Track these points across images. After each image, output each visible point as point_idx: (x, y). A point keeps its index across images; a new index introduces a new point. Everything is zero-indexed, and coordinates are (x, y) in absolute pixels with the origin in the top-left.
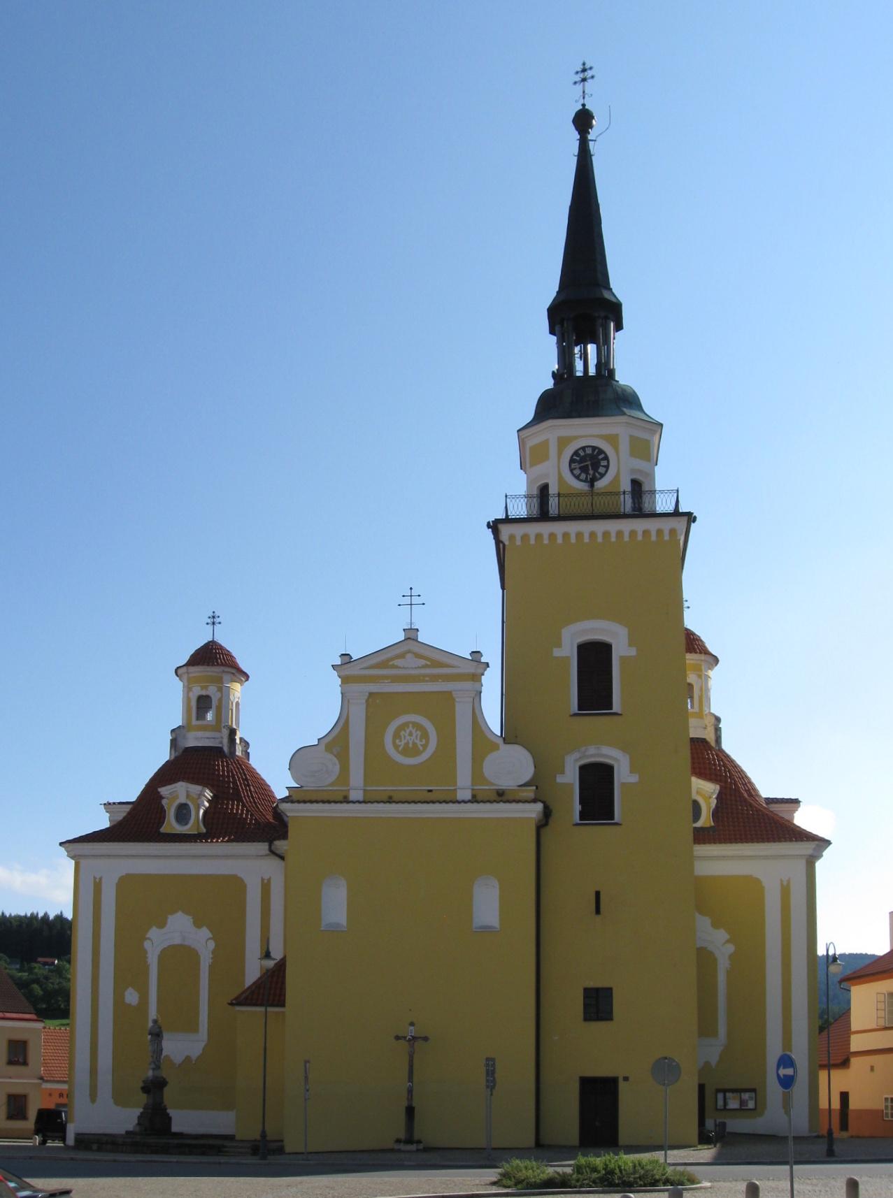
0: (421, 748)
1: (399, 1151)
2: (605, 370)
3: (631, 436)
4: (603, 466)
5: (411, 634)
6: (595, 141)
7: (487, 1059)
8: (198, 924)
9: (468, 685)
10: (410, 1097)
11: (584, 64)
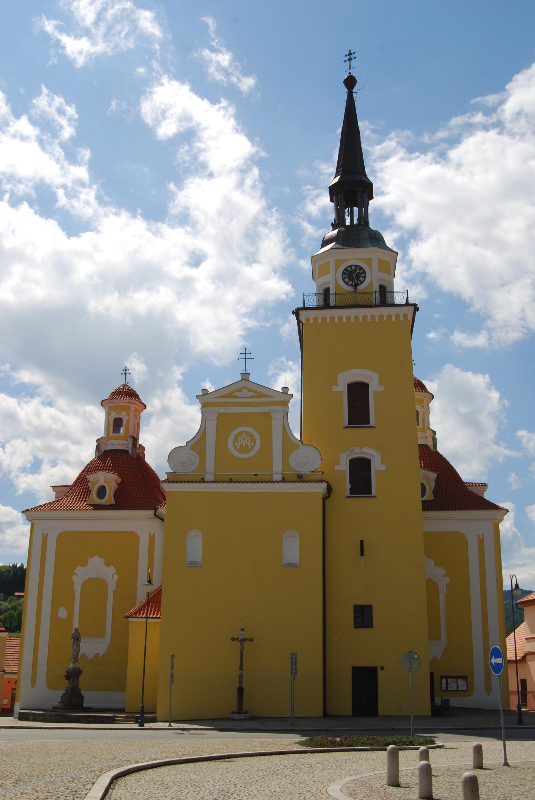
0: (251, 448)
1: (233, 719)
2: (363, 221)
3: (379, 260)
4: (362, 277)
5: (245, 377)
6: (357, 93)
7: (291, 654)
8: (107, 564)
9: (280, 408)
10: (240, 681)
11: (350, 51)
